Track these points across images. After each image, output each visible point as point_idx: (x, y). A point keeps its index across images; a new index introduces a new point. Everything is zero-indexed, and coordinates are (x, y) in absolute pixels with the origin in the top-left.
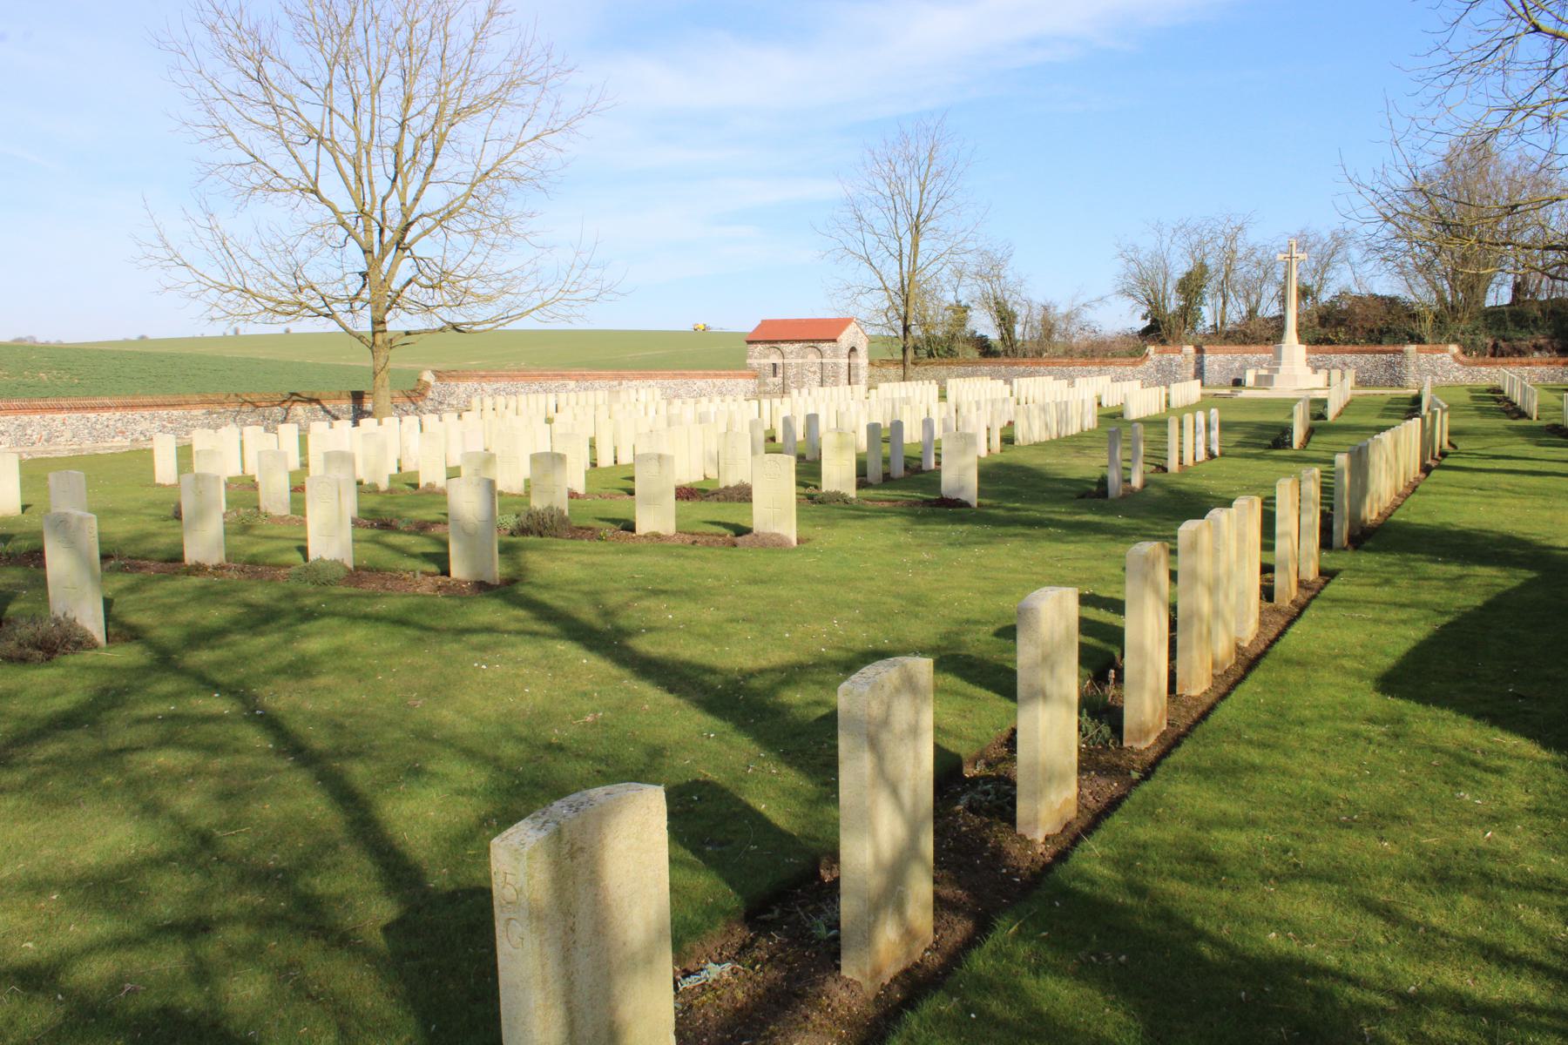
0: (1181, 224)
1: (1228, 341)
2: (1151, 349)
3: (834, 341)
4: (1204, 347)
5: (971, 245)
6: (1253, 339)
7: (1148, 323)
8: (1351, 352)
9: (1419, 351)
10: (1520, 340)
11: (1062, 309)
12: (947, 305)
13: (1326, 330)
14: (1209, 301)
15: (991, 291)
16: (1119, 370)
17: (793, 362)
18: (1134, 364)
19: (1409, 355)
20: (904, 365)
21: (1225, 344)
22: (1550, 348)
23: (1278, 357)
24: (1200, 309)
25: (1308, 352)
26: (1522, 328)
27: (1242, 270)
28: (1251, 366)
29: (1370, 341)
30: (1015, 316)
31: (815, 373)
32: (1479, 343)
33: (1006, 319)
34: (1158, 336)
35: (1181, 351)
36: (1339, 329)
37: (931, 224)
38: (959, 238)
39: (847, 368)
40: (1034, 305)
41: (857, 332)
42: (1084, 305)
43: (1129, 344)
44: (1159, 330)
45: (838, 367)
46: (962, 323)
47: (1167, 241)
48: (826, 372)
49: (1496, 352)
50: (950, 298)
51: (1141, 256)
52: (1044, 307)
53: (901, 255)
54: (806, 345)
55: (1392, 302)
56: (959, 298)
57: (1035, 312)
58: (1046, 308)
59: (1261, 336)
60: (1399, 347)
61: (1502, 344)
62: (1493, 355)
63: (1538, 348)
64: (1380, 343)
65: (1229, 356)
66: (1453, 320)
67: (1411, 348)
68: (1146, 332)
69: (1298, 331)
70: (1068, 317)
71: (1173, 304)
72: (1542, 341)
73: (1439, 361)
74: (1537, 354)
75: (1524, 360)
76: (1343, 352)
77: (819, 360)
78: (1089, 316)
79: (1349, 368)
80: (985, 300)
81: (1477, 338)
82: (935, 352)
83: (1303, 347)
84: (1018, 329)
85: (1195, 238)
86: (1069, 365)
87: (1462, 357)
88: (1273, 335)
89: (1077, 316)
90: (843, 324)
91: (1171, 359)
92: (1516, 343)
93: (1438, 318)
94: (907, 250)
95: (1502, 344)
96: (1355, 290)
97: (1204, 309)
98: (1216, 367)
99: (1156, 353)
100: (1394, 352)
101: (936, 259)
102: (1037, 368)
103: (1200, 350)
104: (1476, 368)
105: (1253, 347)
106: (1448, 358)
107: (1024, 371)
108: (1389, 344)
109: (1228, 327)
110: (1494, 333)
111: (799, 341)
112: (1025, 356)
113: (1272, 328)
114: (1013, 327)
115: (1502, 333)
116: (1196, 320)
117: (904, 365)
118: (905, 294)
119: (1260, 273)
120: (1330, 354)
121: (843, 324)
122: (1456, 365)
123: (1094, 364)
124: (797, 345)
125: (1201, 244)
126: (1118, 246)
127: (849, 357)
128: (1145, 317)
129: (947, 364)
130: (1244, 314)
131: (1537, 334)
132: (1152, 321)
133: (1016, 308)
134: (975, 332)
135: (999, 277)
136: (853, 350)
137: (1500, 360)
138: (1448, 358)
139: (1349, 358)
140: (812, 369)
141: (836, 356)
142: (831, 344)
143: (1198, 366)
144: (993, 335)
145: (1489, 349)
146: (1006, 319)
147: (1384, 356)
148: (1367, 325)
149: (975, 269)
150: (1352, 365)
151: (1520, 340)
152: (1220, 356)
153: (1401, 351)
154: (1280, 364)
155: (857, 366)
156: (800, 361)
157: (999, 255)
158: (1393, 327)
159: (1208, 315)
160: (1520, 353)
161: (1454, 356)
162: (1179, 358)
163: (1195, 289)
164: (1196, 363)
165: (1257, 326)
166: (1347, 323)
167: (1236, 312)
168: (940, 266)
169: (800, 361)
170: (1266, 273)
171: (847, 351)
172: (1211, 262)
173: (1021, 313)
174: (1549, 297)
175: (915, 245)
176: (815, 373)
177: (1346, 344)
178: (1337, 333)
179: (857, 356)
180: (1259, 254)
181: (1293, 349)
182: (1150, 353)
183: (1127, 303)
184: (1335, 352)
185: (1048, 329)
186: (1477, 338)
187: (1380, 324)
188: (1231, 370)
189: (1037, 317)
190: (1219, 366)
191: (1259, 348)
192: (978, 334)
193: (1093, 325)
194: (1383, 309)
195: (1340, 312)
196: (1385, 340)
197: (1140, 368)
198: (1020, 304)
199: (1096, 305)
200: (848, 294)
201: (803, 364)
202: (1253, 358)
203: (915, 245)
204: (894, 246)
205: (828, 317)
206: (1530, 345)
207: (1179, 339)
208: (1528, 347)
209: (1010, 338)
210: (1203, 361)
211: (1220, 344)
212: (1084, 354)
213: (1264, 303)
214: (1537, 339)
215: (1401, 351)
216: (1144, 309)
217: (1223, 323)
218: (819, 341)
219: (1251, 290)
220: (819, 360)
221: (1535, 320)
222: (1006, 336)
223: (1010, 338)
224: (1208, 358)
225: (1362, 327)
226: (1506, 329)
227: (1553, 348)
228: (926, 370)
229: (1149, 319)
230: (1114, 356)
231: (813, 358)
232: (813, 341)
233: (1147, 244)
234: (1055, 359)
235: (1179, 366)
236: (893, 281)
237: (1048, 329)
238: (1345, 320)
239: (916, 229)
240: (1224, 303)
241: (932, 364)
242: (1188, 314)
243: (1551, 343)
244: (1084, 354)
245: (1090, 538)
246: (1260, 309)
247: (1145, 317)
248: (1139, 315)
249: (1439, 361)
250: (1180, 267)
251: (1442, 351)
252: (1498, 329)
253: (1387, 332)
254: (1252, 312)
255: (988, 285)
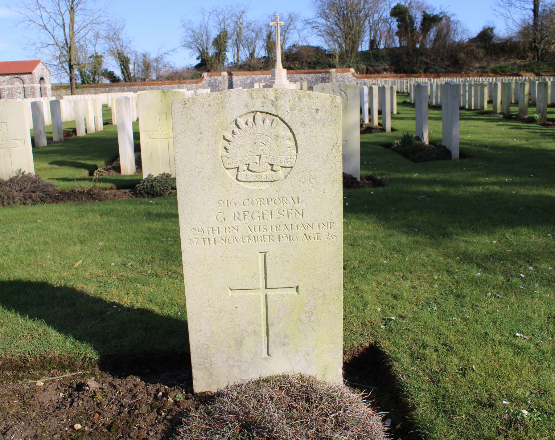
0: (214, 9)
1: (241, 69)
2: (205, 74)
3: (31, 73)
4: (232, 72)
5: (103, 19)
6: (254, 68)
7: (199, 62)
8: (304, 73)
9: (337, 72)
10: (378, 66)
11: (153, 56)
12: (90, 55)
13: (289, 63)
14: (231, 50)
15: (114, 47)
16: (189, 86)
17: (6, 87)
18: (197, 83)
19: (333, 74)
20: (72, 88)
21: (240, 71)
22: (390, 70)
23: (273, 75)
24: (225, 54)
25: (288, 73)
26: (377, 61)
27: (245, 33)
28: (256, 82)
29: (310, 68)
30: (129, 60)
31: (20, 93)
32: (360, 68)
33: (124, 62)
34: (206, 68)
35: (220, 75)
36: (295, 62)
37: (80, 6)
38: (96, 16)
39: (39, 89)
40: (139, 54)
41: (43, 69)
42: (165, 53)
43: (191, 73)
44: (206, 65)
45: (34, 89)
46: (100, 64)
47: (207, 19)
48: (27, 92)
49: (368, 72)
50: (91, 50)
51: (194, 26)
52: (144, 55)
53: (64, 24)
54: (13, 76)
55: (318, 49)
56: (97, 51)
57: (139, 58)
58: (144, 56)
59: (258, 67)
60: (327, 70)
61: (370, 68)
62: (367, 73)
63: (385, 70)
64: (315, 68)
65: (245, 77)
66: (347, 57)
67: (333, 70)
68: (198, 67)
69: (282, 62)
70: (157, 60)
71: (211, 51)
72: (387, 67)
73: (346, 76)
74: (385, 73)
75: (381, 75)
76: (300, 73)
77: (22, 86)
78: (168, 59)
79: (304, 81)
80: (111, 52)
81: (359, 65)
82: (86, 82)
83: (285, 70)
84: (131, 67)
85: (221, 17)
86: (161, 84)
87: (356, 75)
88: (264, 66)
89: (161, 59)
90: (35, 63)
91: (216, 79)
92: (377, 68)
93: (341, 57)
94: (67, 21)
95: (370, 68)
96: (301, 44)
97: (227, 54)
98: (239, 83)
99: (207, 76)
100: (326, 72)
101: (85, 27)
102: (145, 87)
103: (230, 74)
104: (363, 80)
105: (256, 72)
106: (350, 75)
107: (138, 89)
108: (319, 68)
109: (240, 63)
110: (366, 63)
111: (8, 74)
112: (135, 81)
113: (263, 63)
114: (128, 66)
115: (369, 63)
116: (224, 60)
117: (72, 88)
118: (69, 47)
119: (254, 35)
120: (294, 74)
121: (35, 63)
122: (354, 78)
123: (175, 83)
124: (7, 77)
125: (224, 20)
126: (182, 21)
127: (40, 83)
128: (198, 59)
129: (95, 87)
130: (248, 56)
131: (384, 64)
132: (201, 61)
133: (129, 56)
134: (107, 70)
135: (119, 39)
136: (42, 79)
137: (369, 75)
138: (350, 75)
139: (303, 76)
140: (18, 91)
141: (32, 82)
142: (29, 75)
143: (230, 82)
144: (118, 73)
145: (365, 71)
146: (124, 62)
147: (320, 75)
148: (309, 60)
149: (105, 35)
150: (305, 80)
151: (378, 66)
152: (240, 77)
153: (328, 72)
154: (275, 79)
155: (45, 89)
156: (10, 86)
157: (118, 27)
158: (321, 61)
159: (230, 57)
160: (379, 72)
161: (353, 74)
162: (220, 78)
163: (223, 43)
164: (229, 81)
165: (255, 62)
166: (299, 59)
167: (244, 55)
168: (86, 31)
169: (10, 86)
170: (257, 35)
171: (38, 80)
172: (230, 30)
173: (132, 58)
174: (385, 47)
175: (72, 21)
176: (20, 93)
177: (299, 69)
178: (295, 64)
179: (45, 83)
180: (253, 26)
181: (280, 71)
182: (205, 77)
183: (187, 52)
184: (297, 73)
185: (147, 67)
186: (359, 65)
187: (314, 59)
188: (246, 84)
189: (141, 61)
190: (240, 82)
191: (259, 72)
192: (108, 71)
193: (170, 63)
194: (314, 54)
195: (293, 54)
196: (317, 67)
197: (200, 84)
198: (131, 54)
199: (171, 53)
200: (34, 48)
201: (12, 89)
202: (257, 77)
203: (72, 21)
204: (60, 22)
205: (23, 60)
206: (382, 69)
207: (216, 69)
208: (381, 70)
209: (127, 72)
210: (232, 80)
211: (237, 71)
212: (167, 79)
213: (257, 50)
214: (384, 65)
215: (328, 72)
216: (198, 54)
217: (238, 60)
218: (21, 74)
219: (251, 44)
220: (22, 86)
221: (383, 57)
222: (125, 71)
223: (127, 72)
224: (235, 78)
225: (306, 61)
226: (371, 61)
227: (392, 70)
228: (83, 91)
229: (200, 59)
230: (184, 79)
231: (17, 84)
232: (17, 74)
233: (196, 20)
234: (152, 83)
235: (220, 82)
236: (61, 39)
237: (147, 67)
238: (297, 58)
239: (72, 10)
240: (238, 51)
241: (86, 87)
242: (220, 55)
243: (390, 68)
244: (167, 79)
245: (505, 145)
246: (255, 53)
247: (198, 59)
248: (195, 57)
249: (346, 76)
250: (214, 33)
251: (347, 72)
252: (367, 61)
253: (317, 64)
254: (252, 55)
255: (113, 43)
